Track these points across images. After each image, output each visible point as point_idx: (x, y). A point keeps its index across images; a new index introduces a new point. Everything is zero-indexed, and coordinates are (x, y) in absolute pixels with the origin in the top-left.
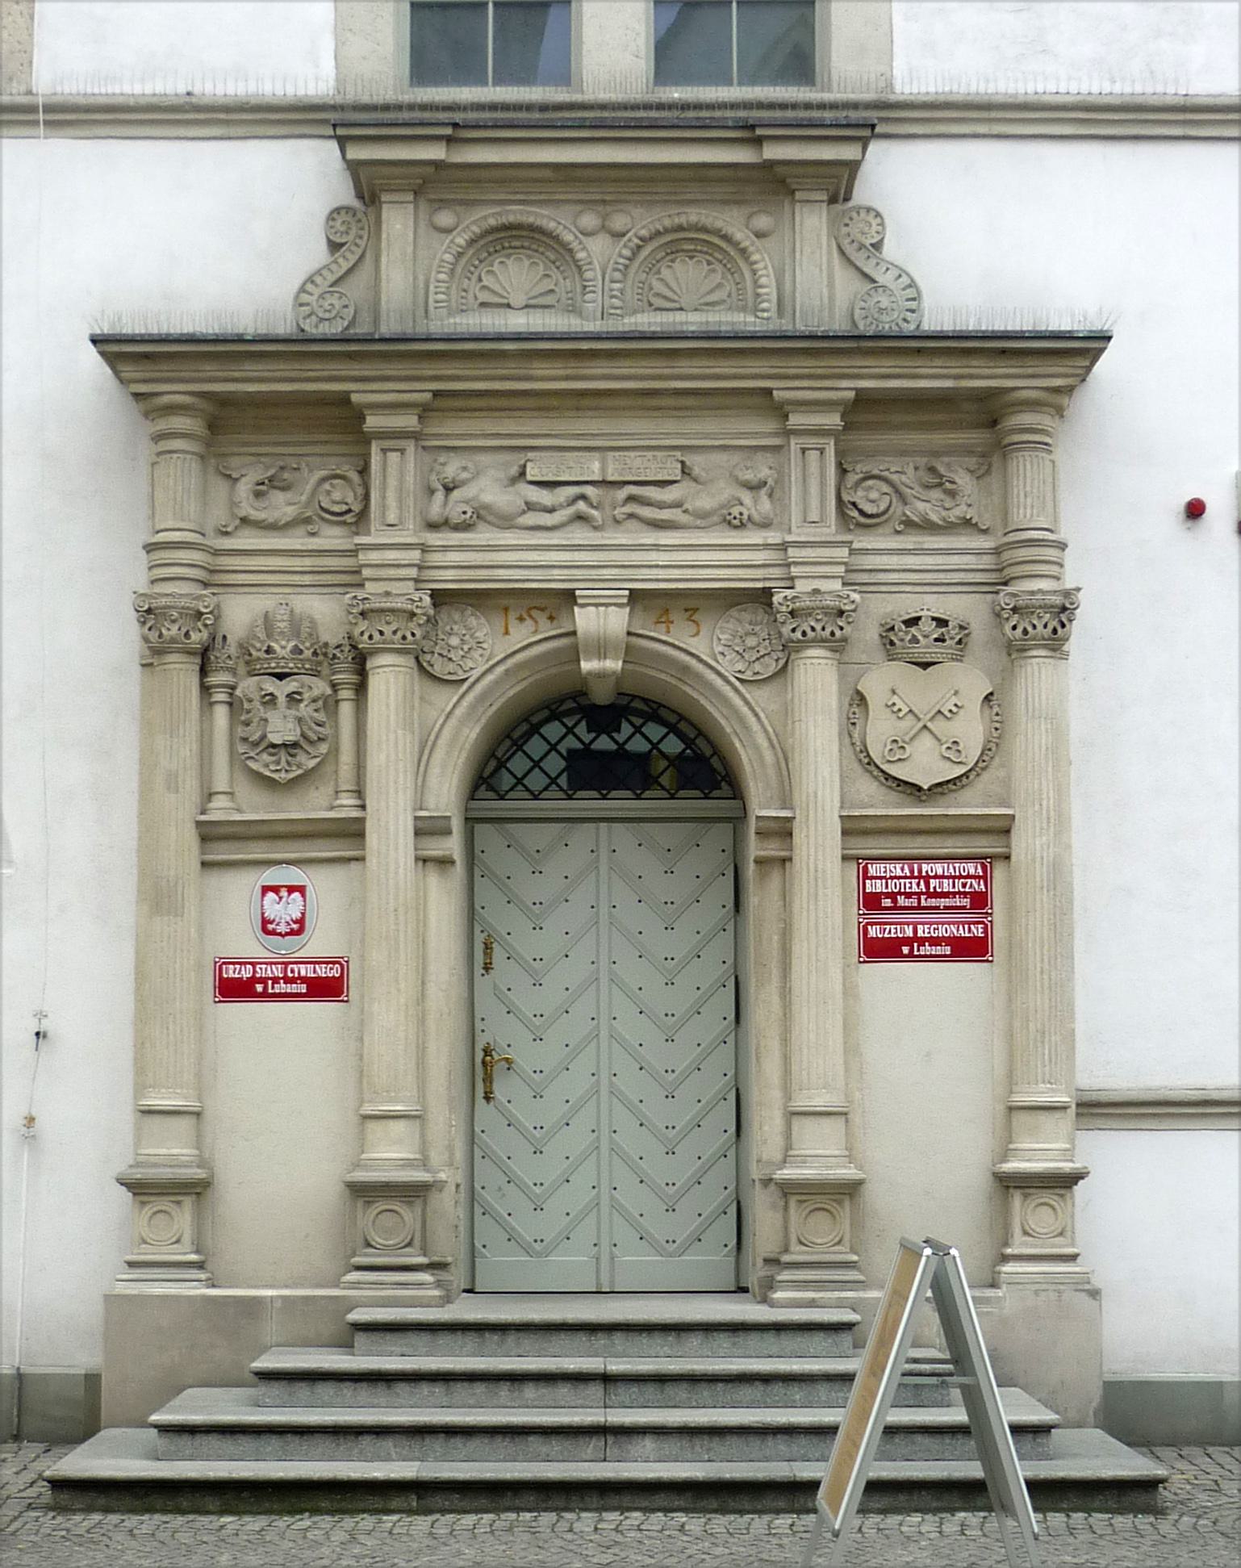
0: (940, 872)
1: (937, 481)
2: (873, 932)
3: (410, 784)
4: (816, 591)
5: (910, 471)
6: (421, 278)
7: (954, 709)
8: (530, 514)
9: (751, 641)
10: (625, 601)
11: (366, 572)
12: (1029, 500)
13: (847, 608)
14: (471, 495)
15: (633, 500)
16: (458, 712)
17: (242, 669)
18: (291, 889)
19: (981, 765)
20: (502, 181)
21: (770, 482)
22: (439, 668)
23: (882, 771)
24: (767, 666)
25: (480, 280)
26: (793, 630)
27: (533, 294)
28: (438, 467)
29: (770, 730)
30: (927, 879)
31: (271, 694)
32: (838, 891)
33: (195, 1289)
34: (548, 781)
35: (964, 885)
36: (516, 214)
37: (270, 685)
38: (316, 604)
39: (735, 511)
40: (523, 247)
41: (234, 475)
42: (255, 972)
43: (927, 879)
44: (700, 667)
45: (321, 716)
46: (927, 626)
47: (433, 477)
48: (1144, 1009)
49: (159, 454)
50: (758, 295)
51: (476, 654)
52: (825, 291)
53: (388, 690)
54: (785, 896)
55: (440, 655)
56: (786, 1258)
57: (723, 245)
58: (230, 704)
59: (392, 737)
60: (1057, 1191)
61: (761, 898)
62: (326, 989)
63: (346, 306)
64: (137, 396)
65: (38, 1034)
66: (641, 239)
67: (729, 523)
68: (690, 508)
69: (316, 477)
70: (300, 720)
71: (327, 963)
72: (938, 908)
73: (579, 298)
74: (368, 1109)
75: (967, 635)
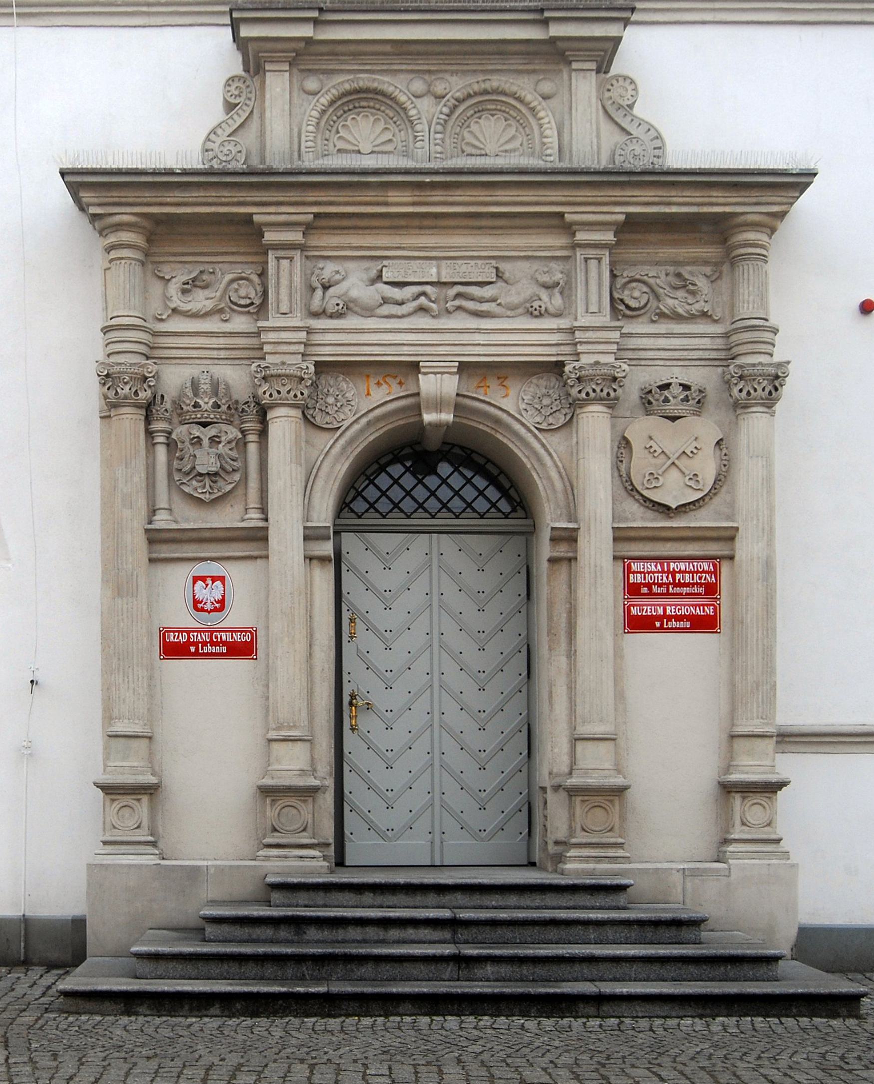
0: (683, 568)
1: (684, 285)
2: (634, 611)
3: (300, 503)
4: (597, 363)
5: (663, 276)
6: (296, 130)
7: (695, 451)
8: (385, 307)
9: (546, 401)
10: (456, 370)
11: (266, 348)
12: (751, 298)
13: (619, 375)
15: (459, 296)
16: (334, 451)
17: (176, 420)
18: (214, 579)
19: (713, 491)
21: (561, 282)
22: (319, 420)
23: (642, 495)
25: (338, 132)
26: (580, 392)
27: (375, 143)
29: (560, 464)
31: (198, 437)
32: (611, 581)
33: (150, 860)
35: (700, 578)
36: (364, 81)
37: (197, 431)
39: (536, 304)
40: (368, 107)
42: (189, 637)
43: (674, 573)
44: (509, 420)
45: (234, 454)
46: (676, 390)
47: (314, 279)
48: (822, 668)
49: (111, 261)
50: (544, 144)
51: (346, 410)
52: (595, 141)
54: (571, 587)
56: (574, 840)
57: (518, 105)
58: (168, 445)
59: (288, 468)
60: (767, 795)
62: (242, 649)
63: (240, 152)
64: (94, 218)
65: (32, 681)
66: (456, 100)
67: (532, 314)
68: (503, 303)
70: (219, 456)
72: (681, 594)
73: (411, 145)
74: (273, 734)
75: (705, 396)
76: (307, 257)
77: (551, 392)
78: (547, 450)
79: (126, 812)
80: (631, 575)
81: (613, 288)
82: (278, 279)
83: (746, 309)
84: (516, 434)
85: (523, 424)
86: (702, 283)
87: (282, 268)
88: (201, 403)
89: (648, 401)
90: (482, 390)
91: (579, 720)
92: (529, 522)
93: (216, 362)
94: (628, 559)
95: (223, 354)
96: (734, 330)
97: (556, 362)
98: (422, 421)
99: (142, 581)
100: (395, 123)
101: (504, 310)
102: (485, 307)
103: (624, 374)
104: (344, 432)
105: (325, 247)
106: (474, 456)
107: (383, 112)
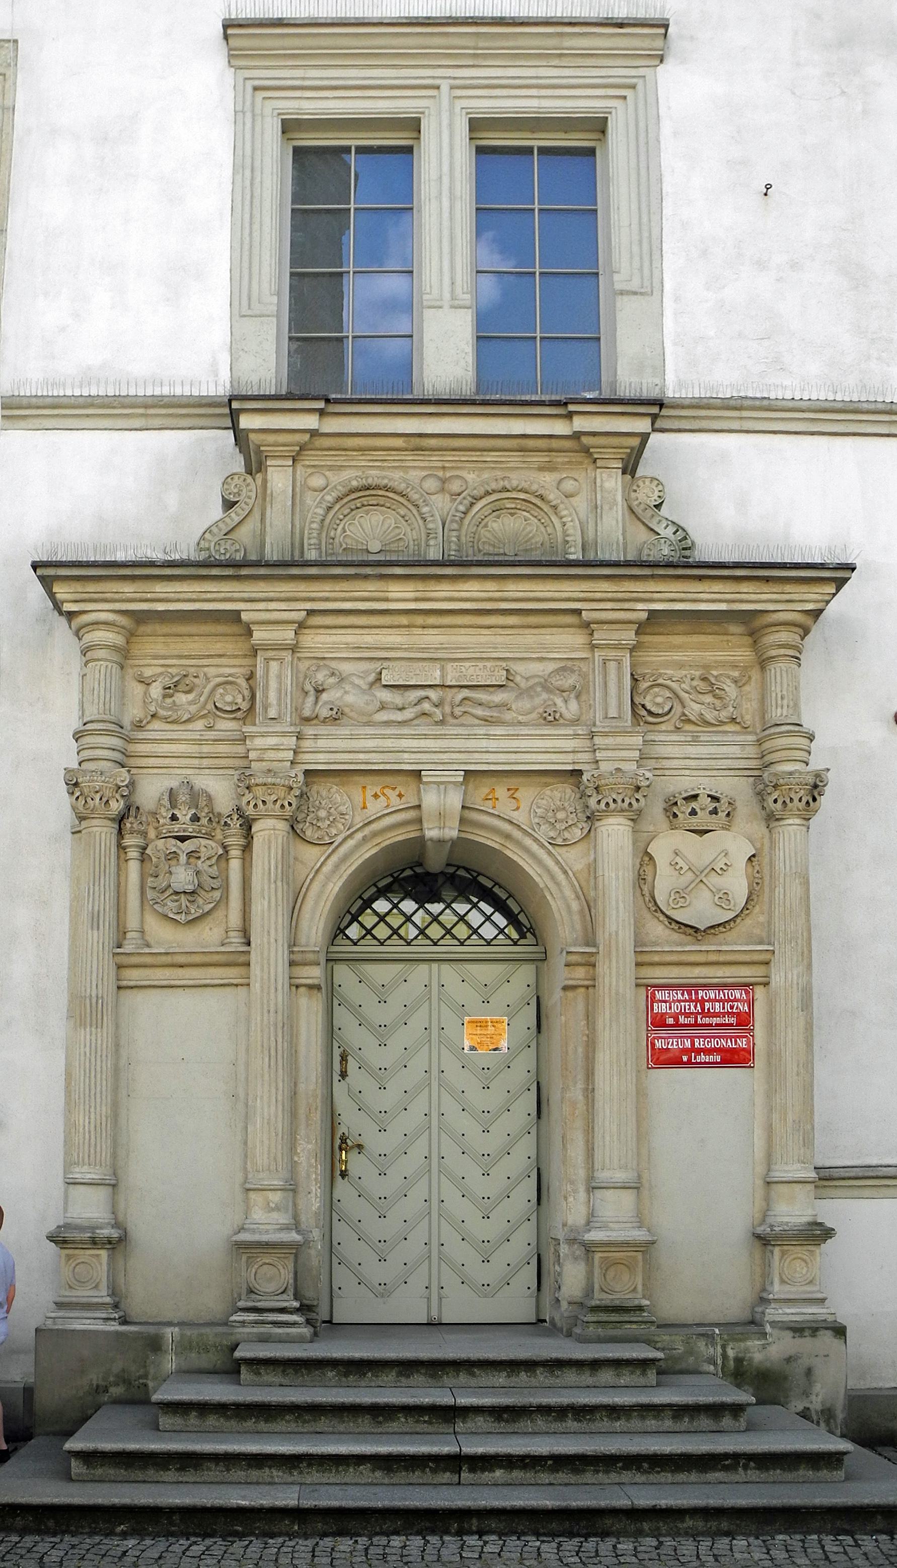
0: (712, 996)
2: (658, 1044)
7: (725, 868)
10: (461, 779)
16: (326, 869)
23: (667, 917)
30: (702, 1002)
34: (390, 932)
35: (732, 1007)
36: (374, 476)
38: (211, 783)
43: (702, 1002)
50: (567, 542)
52: (621, 538)
54: (590, 1017)
58: (142, 861)
66: (473, 497)
67: (545, 719)
70: (198, 873)
72: (711, 1025)
77: (566, 804)
81: (634, 693)
85: (536, 840)
94: (652, 986)
96: (766, 736)
98: (424, 836)
103: (648, 783)
104: (337, 847)
106: (481, 879)
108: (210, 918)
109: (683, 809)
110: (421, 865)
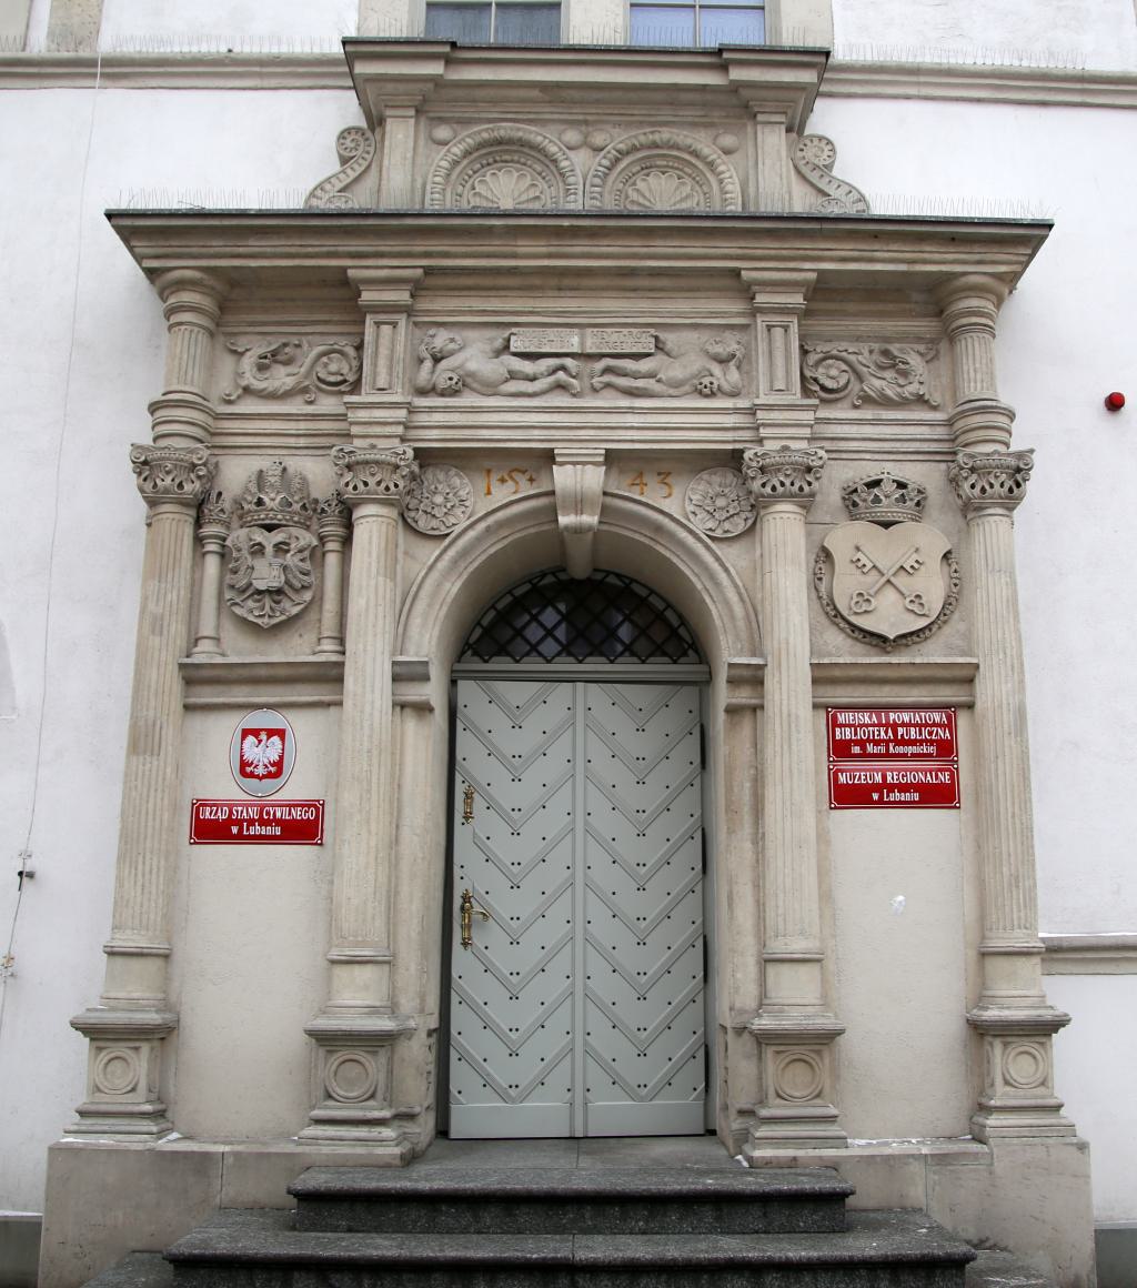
0: (907, 719)
1: (891, 362)
2: (842, 779)
5: (866, 353)
7: (916, 566)
9: (721, 502)
10: (601, 459)
14: (456, 364)
15: (610, 368)
16: (441, 565)
18: (271, 733)
20: (493, 102)
21: (738, 353)
22: (423, 524)
24: (737, 525)
26: (764, 485)
28: (426, 340)
31: (260, 544)
32: (810, 736)
35: (930, 733)
36: (506, 130)
37: (259, 536)
39: (706, 381)
40: (512, 161)
41: (240, 350)
42: (231, 813)
43: (895, 726)
45: (307, 566)
46: (888, 487)
51: (458, 511)
53: (370, 537)
55: (425, 512)
56: (764, 1113)
57: (694, 160)
58: (222, 556)
59: (373, 583)
60: (1037, 1039)
61: (729, 745)
62: (302, 829)
66: (617, 151)
67: (700, 393)
68: (664, 378)
69: (314, 350)
70: (285, 568)
71: (303, 806)
72: (905, 755)
74: (335, 954)
76: (416, 324)
77: (726, 491)
78: (722, 565)
79: (117, 1066)
80: (838, 730)
82: (377, 348)
83: (973, 389)
84: (681, 544)
85: (691, 532)
86: (915, 362)
87: (382, 334)
88: (266, 499)
89: (852, 502)
90: (637, 488)
91: (770, 933)
92: (703, 668)
93: (294, 452)
95: (302, 442)
97: (733, 450)
99: (169, 734)
100: (544, 178)
101: (665, 388)
102: (640, 383)
103: (821, 463)
105: (438, 311)
106: (635, 587)
107: (530, 167)
108: (300, 623)
109: (864, 495)
110: (564, 570)
